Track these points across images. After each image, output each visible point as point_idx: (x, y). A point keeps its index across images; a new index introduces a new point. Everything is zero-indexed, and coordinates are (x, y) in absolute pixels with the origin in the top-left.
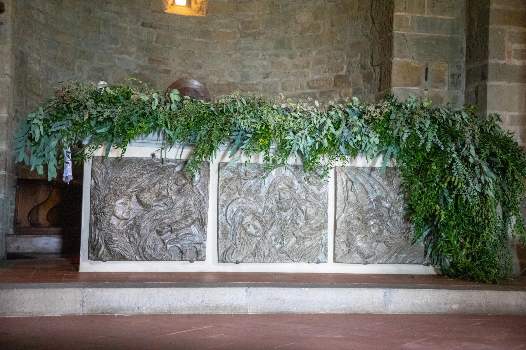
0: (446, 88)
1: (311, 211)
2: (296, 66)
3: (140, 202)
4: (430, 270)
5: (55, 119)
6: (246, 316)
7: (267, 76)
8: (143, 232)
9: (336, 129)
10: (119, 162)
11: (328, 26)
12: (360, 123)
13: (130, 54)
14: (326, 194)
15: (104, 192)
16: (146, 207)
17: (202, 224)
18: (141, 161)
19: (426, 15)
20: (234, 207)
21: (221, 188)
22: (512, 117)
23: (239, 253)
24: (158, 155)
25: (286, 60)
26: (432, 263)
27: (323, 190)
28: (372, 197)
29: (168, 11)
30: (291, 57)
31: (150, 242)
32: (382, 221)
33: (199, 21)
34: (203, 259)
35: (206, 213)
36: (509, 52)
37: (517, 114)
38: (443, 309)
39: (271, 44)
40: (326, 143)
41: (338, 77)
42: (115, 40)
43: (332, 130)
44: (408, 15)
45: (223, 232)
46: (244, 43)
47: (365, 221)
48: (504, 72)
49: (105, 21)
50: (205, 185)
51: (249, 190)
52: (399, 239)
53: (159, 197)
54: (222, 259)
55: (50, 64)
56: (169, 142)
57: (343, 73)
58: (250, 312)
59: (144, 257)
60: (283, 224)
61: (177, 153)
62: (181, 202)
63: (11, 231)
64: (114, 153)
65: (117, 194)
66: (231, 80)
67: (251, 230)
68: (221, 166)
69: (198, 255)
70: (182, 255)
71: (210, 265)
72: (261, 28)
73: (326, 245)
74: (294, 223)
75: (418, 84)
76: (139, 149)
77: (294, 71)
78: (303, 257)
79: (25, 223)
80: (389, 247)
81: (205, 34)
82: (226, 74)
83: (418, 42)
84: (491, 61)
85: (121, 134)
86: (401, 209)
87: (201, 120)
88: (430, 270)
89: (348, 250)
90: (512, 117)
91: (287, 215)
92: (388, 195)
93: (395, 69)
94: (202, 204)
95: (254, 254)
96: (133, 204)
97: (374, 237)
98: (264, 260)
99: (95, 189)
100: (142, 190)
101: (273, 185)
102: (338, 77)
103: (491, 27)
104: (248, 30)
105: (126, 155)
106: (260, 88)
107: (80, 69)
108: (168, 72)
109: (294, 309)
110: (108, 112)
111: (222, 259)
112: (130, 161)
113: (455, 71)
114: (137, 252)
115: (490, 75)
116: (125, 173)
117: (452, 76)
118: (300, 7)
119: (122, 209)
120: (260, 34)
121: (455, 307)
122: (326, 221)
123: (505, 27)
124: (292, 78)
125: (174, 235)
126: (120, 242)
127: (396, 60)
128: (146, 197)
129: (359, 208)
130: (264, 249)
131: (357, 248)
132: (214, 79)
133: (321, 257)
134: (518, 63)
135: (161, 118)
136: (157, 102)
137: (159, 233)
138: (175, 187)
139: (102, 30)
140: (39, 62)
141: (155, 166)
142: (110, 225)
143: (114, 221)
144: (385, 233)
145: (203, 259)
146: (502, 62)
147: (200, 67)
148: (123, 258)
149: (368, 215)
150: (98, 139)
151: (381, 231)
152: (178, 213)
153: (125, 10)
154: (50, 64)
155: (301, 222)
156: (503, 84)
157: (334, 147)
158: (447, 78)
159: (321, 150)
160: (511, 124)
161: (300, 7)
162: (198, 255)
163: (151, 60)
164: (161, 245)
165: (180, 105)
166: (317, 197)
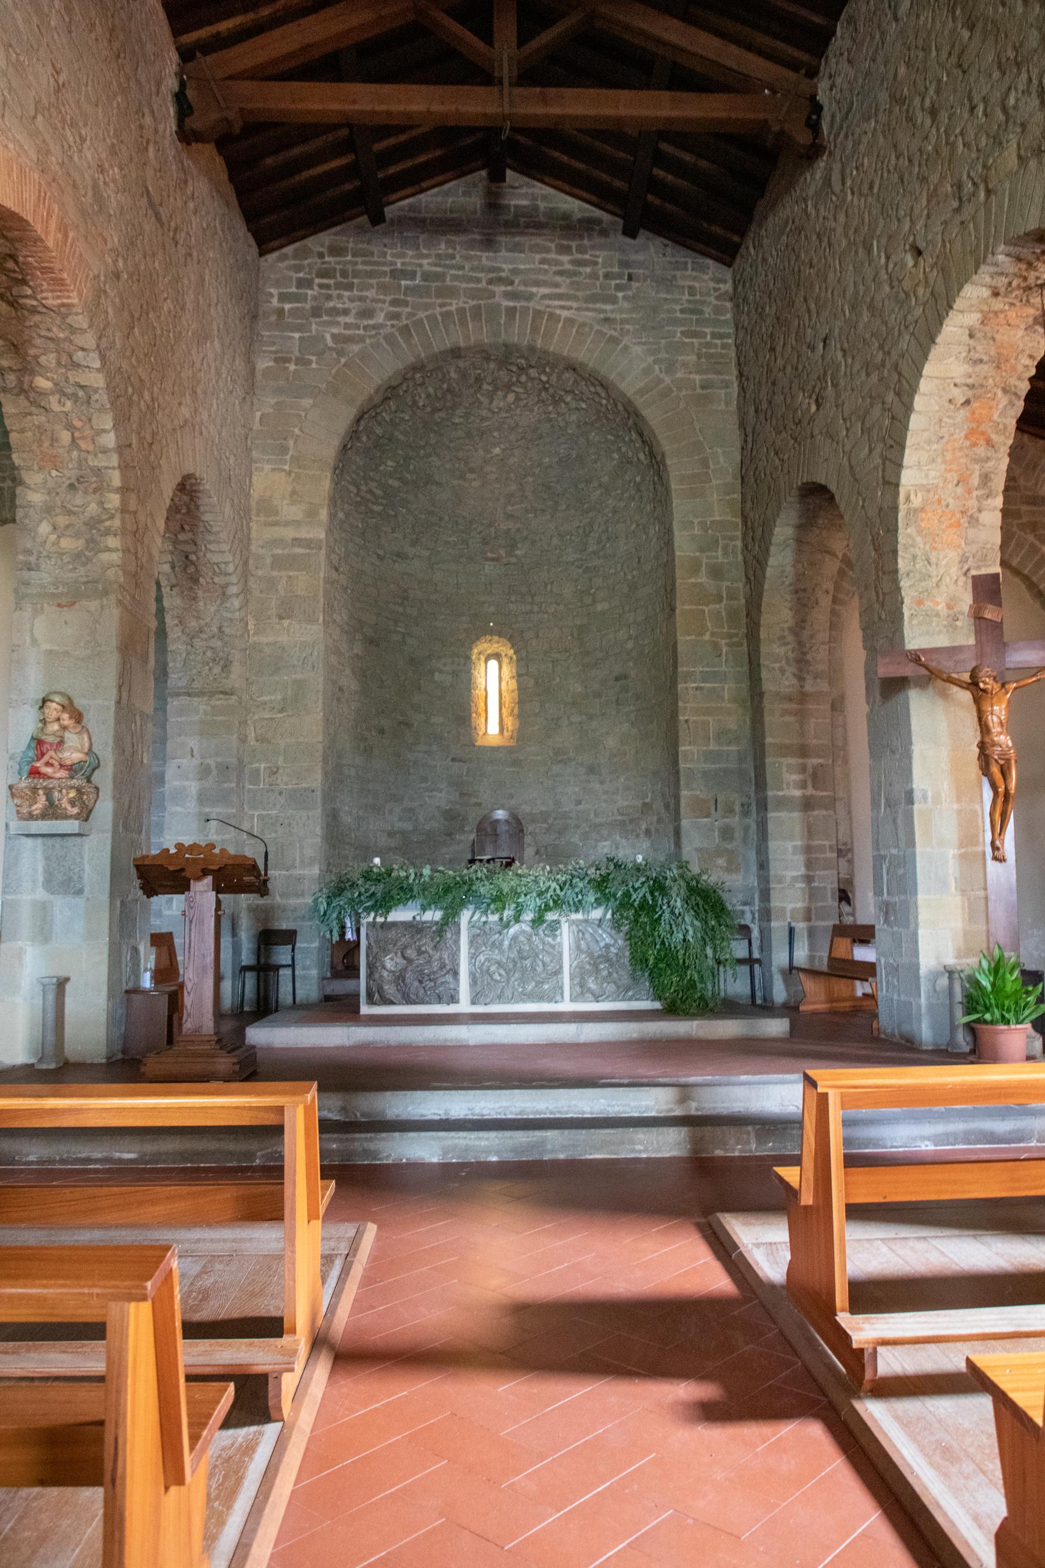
0: (737, 818)
1: (547, 959)
2: (606, 792)
3: (404, 958)
4: (657, 1005)
5: (335, 896)
6: (468, 1047)
7: (579, 802)
8: (408, 981)
9: (561, 889)
10: (386, 926)
11: (633, 752)
12: (581, 885)
13: (441, 791)
14: (560, 944)
15: (375, 950)
16: (410, 961)
17: (456, 973)
18: (404, 924)
19: (711, 747)
20: (482, 958)
21: (471, 943)
22: (795, 847)
23: (486, 996)
24: (418, 918)
25: (597, 786)
26: (659, 998)
27: (559, 939)
28: (602, 944)
29: (479, 742)
30: (602, 783)
31: (413, 990)
32: (611, 965)
33: (510, 750)
34: (458, 1002)
35: (458, 965)
36: (788, 784)
37: (799, 843)
38: (625, 1037)
39: (582, 770)
40: (551, 903)
41: (645, 805)
42: (424, 779)
43: (558, 891)
44: (694, 749)
45: (474, 981)
46: (556, 769)
47: (596, 966)
48: (783, 803)
49: (415, 762)
50: (457, 942)
51: (493, 944)
52: (626, 980)
53: (420, 952)
54: (473, 1003)
55: (361, 813)
56: (424, 909)
57: (648, 800)
58: (471, 1043)
59: (409, 1001)
60: (524, 970)
61: (433, 915)
62: (437, 956)
63: (329, 975)
64: (380, 920)
65: (386, 952)
66: (543, 808)
67: (497, 977)
68: (471, 925)
69: (454, 999)
70: (439, 1000)
71: (464, 1006)
72: (572, 754)
73: (561, 988)
74: (534, 969)
75: (708, 816)
76: (400, 915)
77: (604, 797)
78: (541, 998)
79: (340, 967)
80: (618, 987)
81: (516, 763)
82: (539, 802)
83: (705, 774)
84: (770, 793)
85: (384, 904)
86: (627, 953)
87: (447, 890)
88: (657, 1005)
89: (581, 992)
90: (795, 847)
91: (528, 963)
92: (616, 941)
93: (683, 802)
94: (455, 956)
95: (499, 997)
96: (399, 960)
97: (604, 979)
98: (510, 1001)
99: (369, 947)
100: (406, 947)
101: (514, 938)
102: (645, 805)
103: (767, 760)
104: (560, 756)
105: (389, 919)
106: (573, 815)
107: (391, 811)
108: (479, 805)
109: (505, 1041)
110: (373, 889)
111: (473, 1003)
112: (394, 924)
113: (745, 800)
114: (403, 997)
115: (769, 807)
116: (392, 934)
117: (743, 805)
118: (607, 733)
119: (390, 963)
120: (571, 760)
121: (635, 1035)
122: (561, 967)
123: (782, 760)
124: (604, 805)
125: (429, 982)
126: (390, 989)
127: (684, 793)
128: (411, 953)
129: (590, 954)
130: (508, 993)
131: (589, 990)
132: (526, 808)
133: (558, 998)
134: (798, 793)
135: (415, 888)
136: (413, 876)
137: (421, 982)
138: (432, 945)
139: (412, 771)
140: (350, 813)
141: (414, 928)
142: (381, 976)
143: (385, 974)
144: (615, 975)
145: (458, 1002)
146: (780, 793)
147: (511, 797)
148: (392, 1003)
149: (595, 963)
150: (368, 910)
151: (610, 974)
152: (436, 965)
153: (435, 747)
154: (361, 813)
155: (539, 969)
156: (783, 815)
157: (558, 903)
158: (737, 808)
159: (548, 908)
160: (794, 853)
161: (607, 733)
162: (454, 999)
163: (462, 795)
164: (422, 991)
165: (432, 878)
166: (553, 947)
